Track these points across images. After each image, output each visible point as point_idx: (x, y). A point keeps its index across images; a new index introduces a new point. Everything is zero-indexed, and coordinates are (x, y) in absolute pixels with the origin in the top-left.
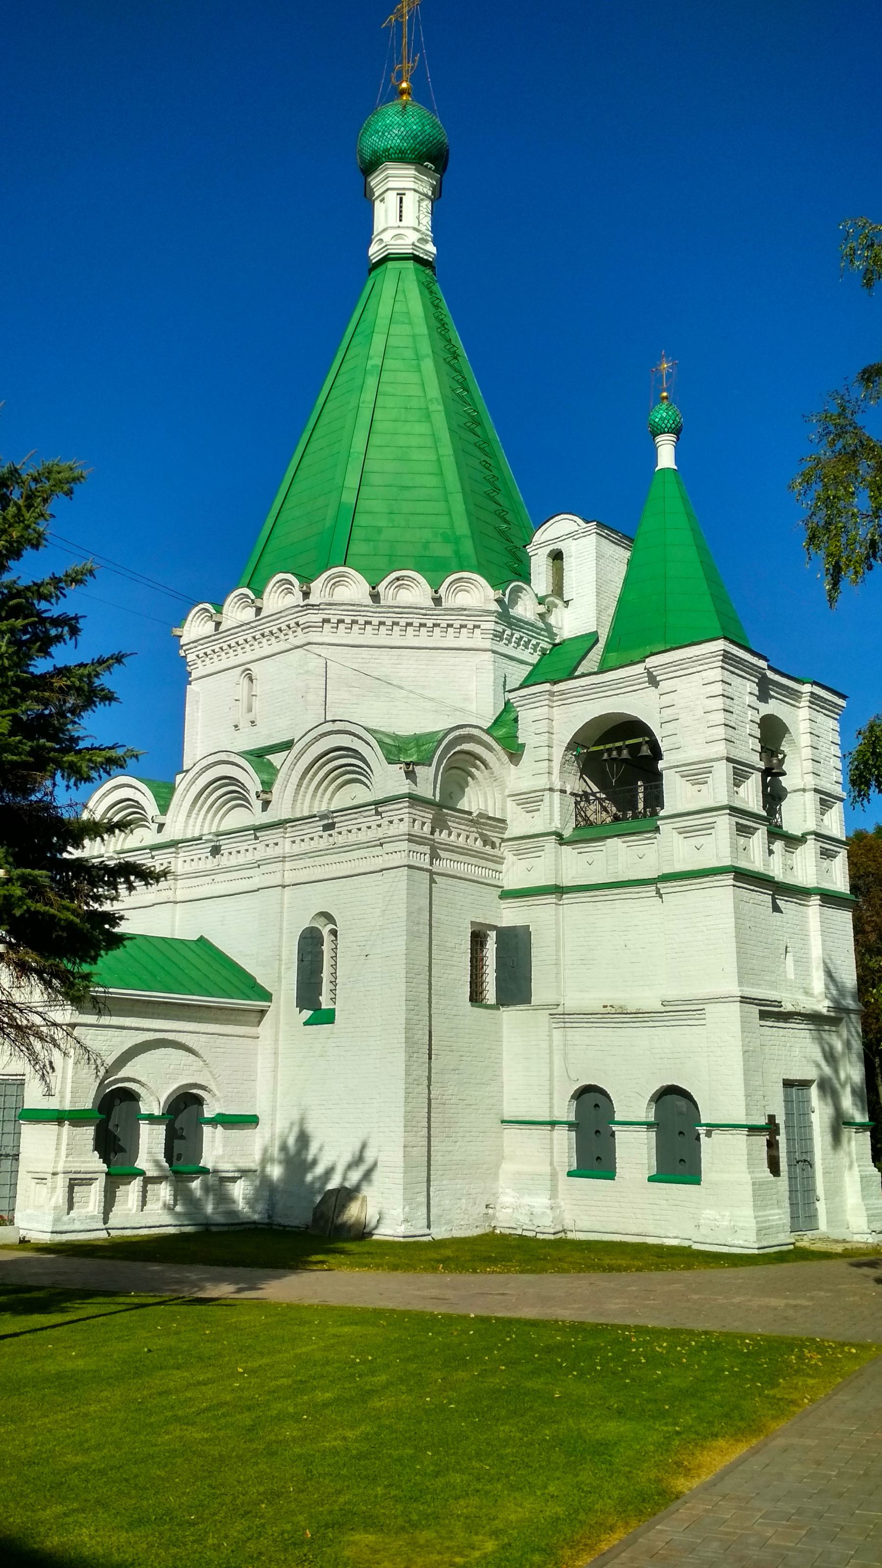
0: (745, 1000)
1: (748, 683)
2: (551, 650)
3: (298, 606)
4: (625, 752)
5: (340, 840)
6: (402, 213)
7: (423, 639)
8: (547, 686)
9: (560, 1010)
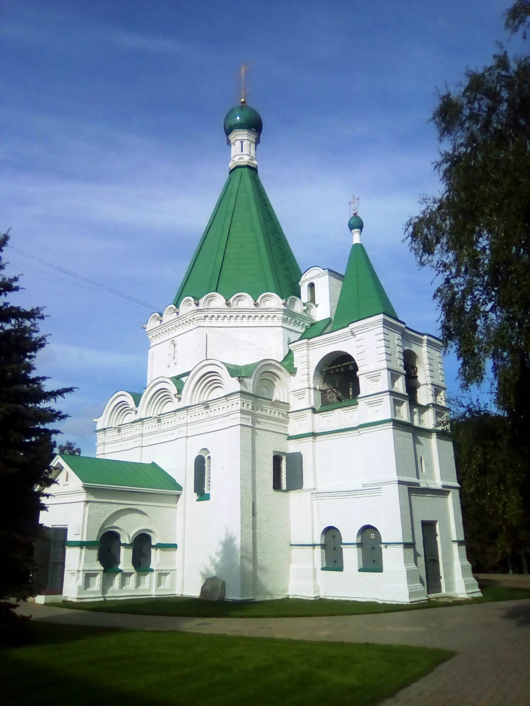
1: (396, 335)
2: (310, 327)
3: (194, 310)
4: (342, 369)
5: (212, 414)
7: (251, 323)
8: (306, 340)
9: (315, 492)
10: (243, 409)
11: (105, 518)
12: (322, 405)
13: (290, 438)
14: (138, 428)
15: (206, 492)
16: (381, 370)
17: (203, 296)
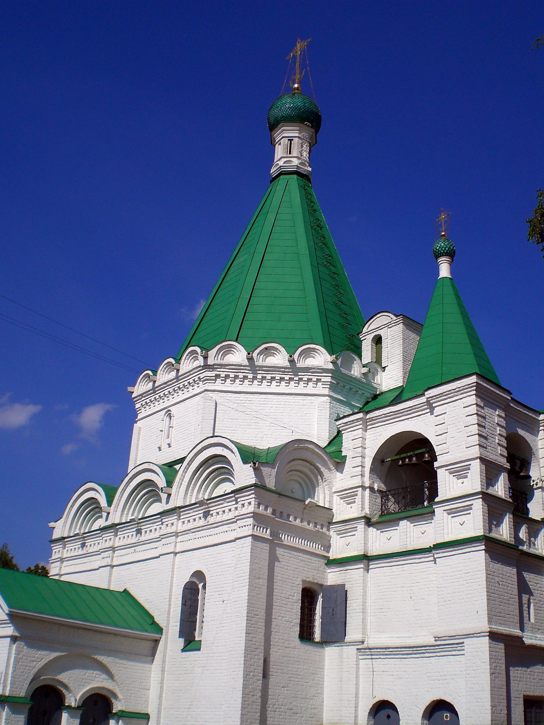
4: (414, 459)
6: (290, 150)
8: (361, 415)
9: (365, 645)
10: (257, 511)
12: (381, 516)
13: (331, 563)
15: (197, 639)
17: (215, 347)
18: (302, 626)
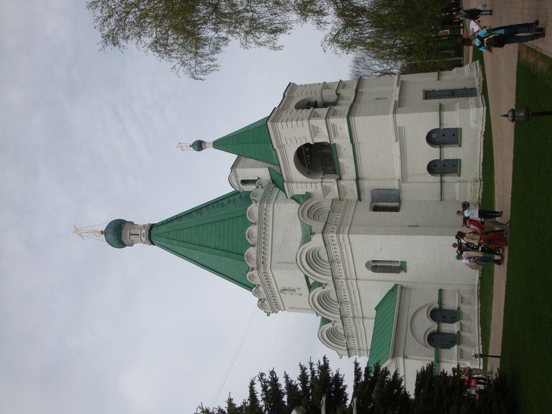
0: (394, 112)
7: (270, 228)
8: (285, 184)
9: (401, 179)
10: (336, 232)
11: (417, 343)
12: (336, 174)
13: (360, 199)
14: (349, 321)
15: (400, 265)
16: (309, 125)
18: (392, 211)
